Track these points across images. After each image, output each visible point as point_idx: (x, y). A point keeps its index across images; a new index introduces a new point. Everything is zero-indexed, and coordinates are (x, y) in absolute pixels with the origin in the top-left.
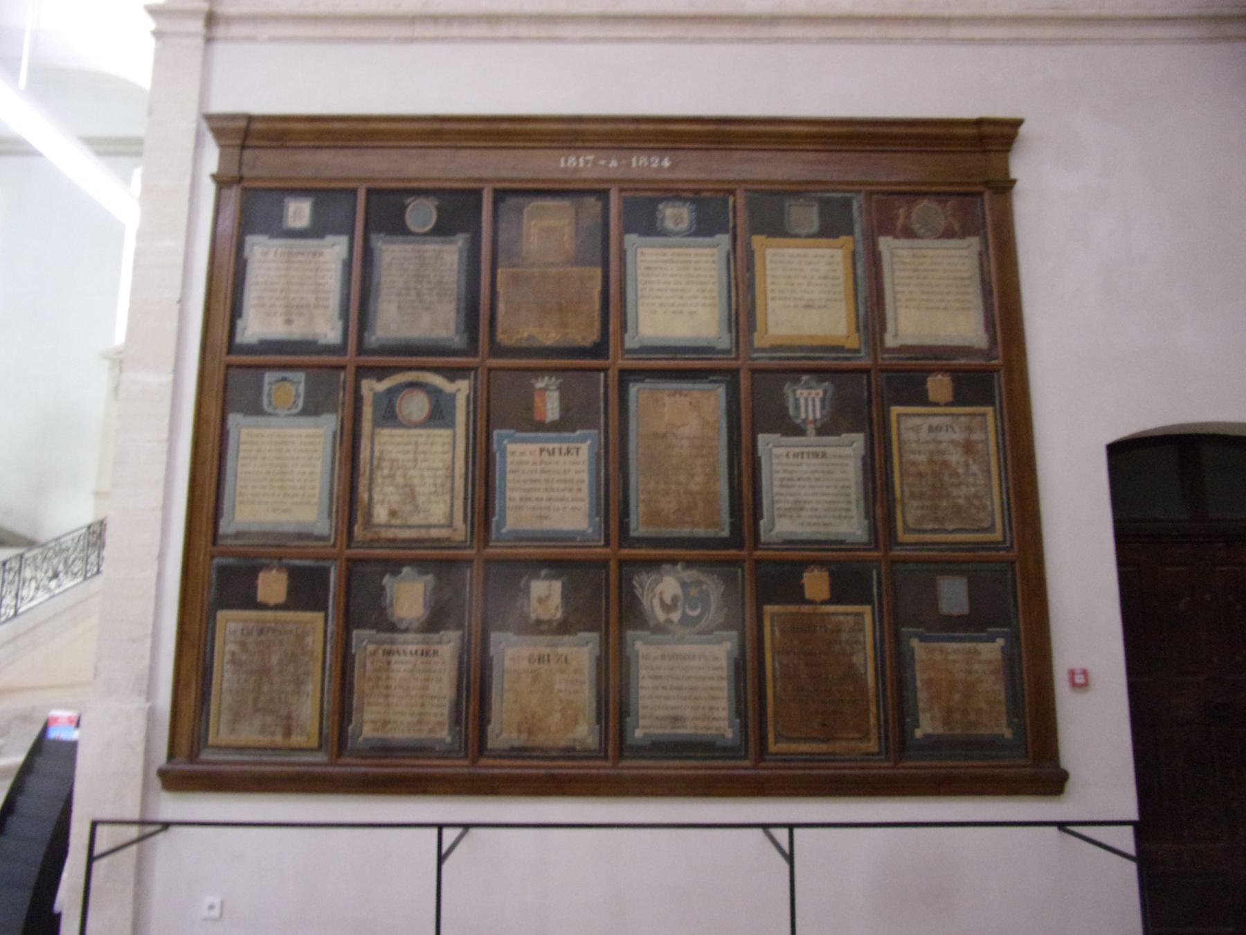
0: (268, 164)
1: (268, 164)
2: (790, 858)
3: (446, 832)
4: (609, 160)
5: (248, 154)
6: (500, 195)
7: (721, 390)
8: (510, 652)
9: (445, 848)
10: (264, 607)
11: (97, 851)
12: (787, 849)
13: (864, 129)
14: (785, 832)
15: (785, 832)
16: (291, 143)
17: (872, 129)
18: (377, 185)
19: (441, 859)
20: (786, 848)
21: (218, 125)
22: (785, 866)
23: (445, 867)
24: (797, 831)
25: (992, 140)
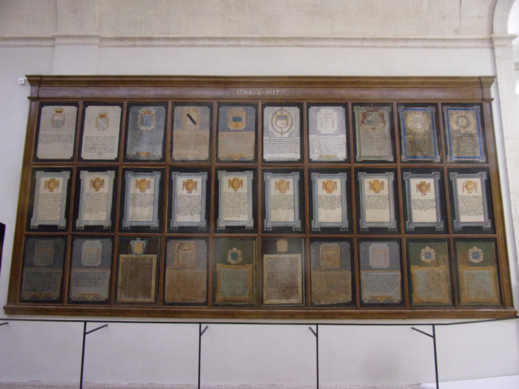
0: (46, 92)
1: (46, 92)
2: (317, 335)
3: (202, 325)
4: (248, 91)
5: (41, 88)
6: (443, 104)
7: (69, 172)
8: (465, 272)
9: (202, 331)
10: (280, 253)
11: (87, 331)
12: (316, 332)
13: (116, 79)
14: (315, 326)
15: (315, 326)
16: (362, 86)
17: (101, 79)
18: (444, 102)
19: (201, 334)
20: (315, 332)
21: (29, 79)
22: (315, 338)
23: (202, 337)
24: (319, 326)
25: (483, 83)
